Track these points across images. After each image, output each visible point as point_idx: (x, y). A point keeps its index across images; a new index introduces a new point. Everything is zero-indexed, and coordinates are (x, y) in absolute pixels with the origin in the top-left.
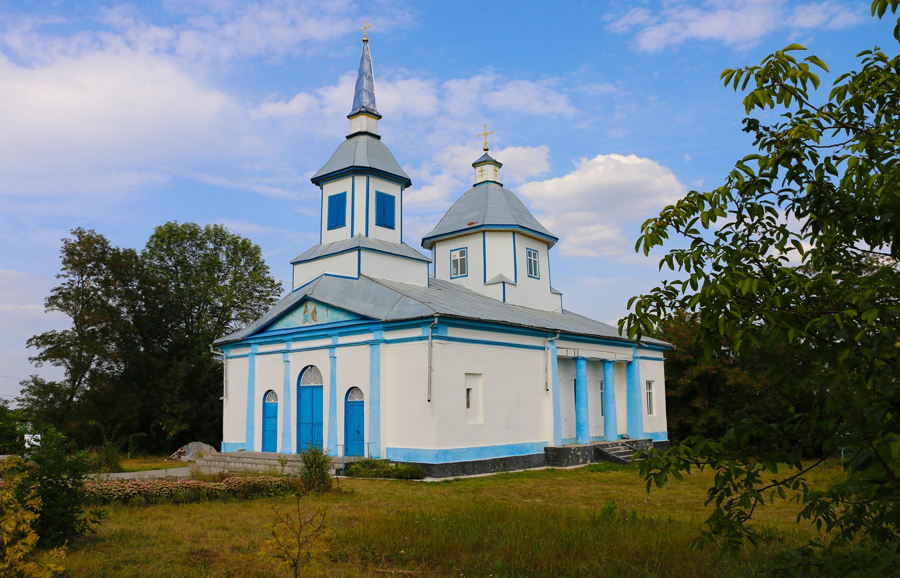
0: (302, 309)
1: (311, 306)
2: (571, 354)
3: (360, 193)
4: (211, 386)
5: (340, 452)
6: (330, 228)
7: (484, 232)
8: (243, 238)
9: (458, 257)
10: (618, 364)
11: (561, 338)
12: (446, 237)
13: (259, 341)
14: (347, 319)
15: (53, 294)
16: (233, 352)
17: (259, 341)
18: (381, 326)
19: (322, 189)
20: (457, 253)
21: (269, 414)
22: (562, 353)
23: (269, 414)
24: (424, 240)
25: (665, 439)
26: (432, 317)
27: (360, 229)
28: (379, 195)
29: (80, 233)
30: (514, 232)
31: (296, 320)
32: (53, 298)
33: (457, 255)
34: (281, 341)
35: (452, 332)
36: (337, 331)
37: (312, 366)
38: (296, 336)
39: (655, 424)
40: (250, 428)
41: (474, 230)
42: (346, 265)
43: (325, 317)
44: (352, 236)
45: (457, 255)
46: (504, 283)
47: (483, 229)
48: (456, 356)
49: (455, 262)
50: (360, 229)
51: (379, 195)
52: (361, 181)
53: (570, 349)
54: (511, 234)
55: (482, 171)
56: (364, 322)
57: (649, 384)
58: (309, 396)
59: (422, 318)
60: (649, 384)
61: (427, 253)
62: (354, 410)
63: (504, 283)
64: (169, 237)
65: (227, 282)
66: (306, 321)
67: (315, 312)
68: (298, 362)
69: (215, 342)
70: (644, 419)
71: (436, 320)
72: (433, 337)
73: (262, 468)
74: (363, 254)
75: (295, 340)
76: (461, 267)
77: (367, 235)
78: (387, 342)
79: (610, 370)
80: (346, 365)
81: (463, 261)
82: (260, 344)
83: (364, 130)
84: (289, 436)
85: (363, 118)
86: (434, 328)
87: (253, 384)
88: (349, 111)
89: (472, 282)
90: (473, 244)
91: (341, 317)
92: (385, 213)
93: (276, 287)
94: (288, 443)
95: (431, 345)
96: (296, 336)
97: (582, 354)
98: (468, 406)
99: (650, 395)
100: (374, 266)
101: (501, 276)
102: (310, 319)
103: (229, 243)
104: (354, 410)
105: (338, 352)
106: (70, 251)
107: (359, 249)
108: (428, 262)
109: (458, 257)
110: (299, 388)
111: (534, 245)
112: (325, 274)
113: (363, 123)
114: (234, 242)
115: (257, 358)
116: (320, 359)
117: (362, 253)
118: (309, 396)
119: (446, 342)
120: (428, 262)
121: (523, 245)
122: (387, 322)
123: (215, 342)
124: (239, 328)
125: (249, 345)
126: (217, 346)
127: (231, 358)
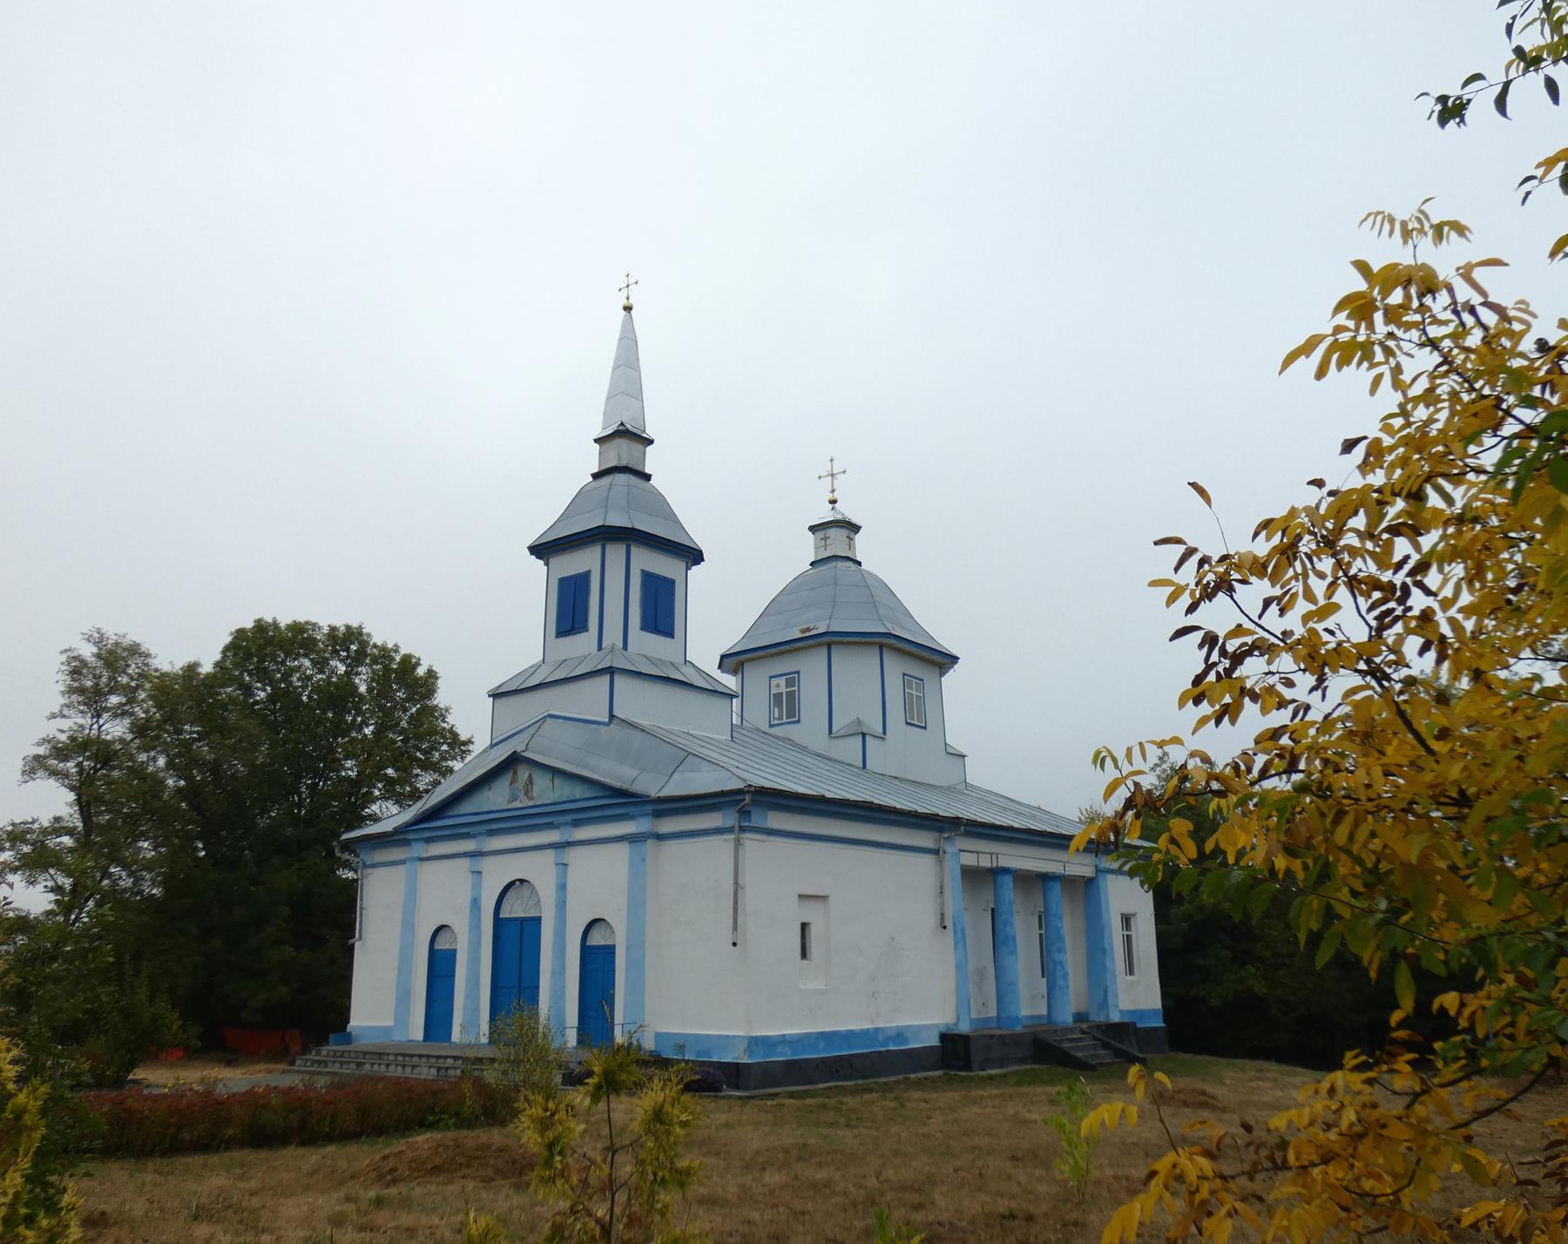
0: (508, 777)
1: (523, 773)
2: (985, 862)
3: (615, 579)
4: (332, 922)
5: (572, 1038)
6: (588, 573)
7: (829, 645)
8: (403, 651)
9: (783, 690)
10: (1069, 882)
11: (967, 834)
12: (761, 653)
13: (426, 835)
14: (588, 795)
15: (41, 751)
16: (381, 856)
17: (426, 835)
18: (649, 808)
19: (547, 564)
20: (782, 682)
21: (441, 967)
22: (969, 860)
23: (441, 967)
24: (723, 657)
25: (1159, 1023)
26: (739, 792)
27: (613, 635)
28: (649, 579)
29: (99, 639)
30: (881, 646)
31: (497, 798)
32: (37, 758)
33: (781, 686)
34: (467, 836)
35: (776, 820)
36: (569, 818)
37: (522, 881)
38: (494, 826)
39: (1138, 992)
40: (404, 997)
41: (811, 642)
42: (589, 700)
43: (546, 791)
44: (600, 648)
45: (781, 686)
46: (864, 735)
47: (827, 639)
48: (780, 866)
49: (778, 697)
50: (613, 635)
51: (649, 579)
52: (616, 553)
53: (983, 854)
54: (824, 651)
55: (825, 539)
56: (618, 801)
57: (1127, 920)
58: (515, 942)
59: (723, 793)
60: (1127, 920)
61: (730, 681)
62: (597, 964)
63: (864, 735)
64: (260, 647)
65: (368, 731)
66: (514, 798)
67: (530, 781)
68: (497, 873)
69: (345, 837)
70: (1121, 987)
71: (748, 798)
72: (742, 829)
73: (427, 1073)
74: (619, 681)
75: (491, 833)
76: (788, 706)
77: (625, 647)
78: (660, 837)
79: (1056, 888)
80: (586, 883)
81: (791, 695)
82: (428, 840)
83: (624, 463)
84: (476, 1010)
85: (622, 443)
86: (744, 813)
87: (409, 928)
88: (599, 432)
89: (811, 728)
90: (811, 667)
91: (579, 791)
92: (660, 607)
93: (458, 746)
94: (472, 1020)
95: (738, 844)
96: (494, 826)
97: (1004, 862)
98: (804, 955)
99: (1128, 940)
100: (635, 701)
101: (859, 722)
102: (522, 795)
103: (375, 660)
104: (597, 964)
105: (575, 856)
106: (77, 668)
107: (611, 671)
108: (732, 696)
109: (783, 690)
110: (498, 922)
111: (914, 669)
112: (551, 716)
113: (622, 452)
114: (385, 654)
115: (427, 866)
116: (539, 869)
117: (618, 679)
118: (515, 942)
119: (763, 837)
120: (732, 696)
121: (896, 668)
122: (660, 800)
123: (345, 837)
124: (388, 815)
125: (407, 843)
126: (348, 846)
127: (373, 866)
